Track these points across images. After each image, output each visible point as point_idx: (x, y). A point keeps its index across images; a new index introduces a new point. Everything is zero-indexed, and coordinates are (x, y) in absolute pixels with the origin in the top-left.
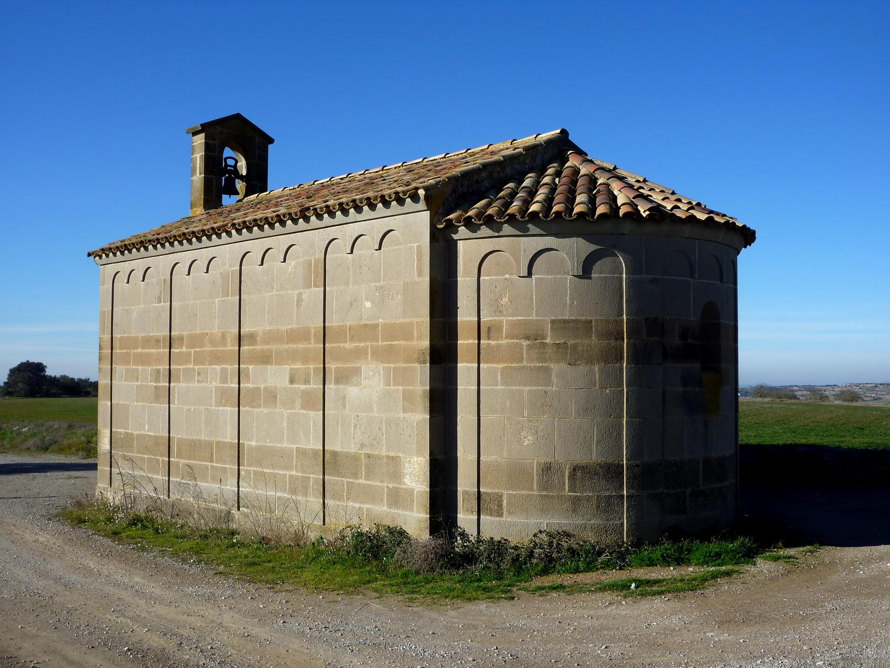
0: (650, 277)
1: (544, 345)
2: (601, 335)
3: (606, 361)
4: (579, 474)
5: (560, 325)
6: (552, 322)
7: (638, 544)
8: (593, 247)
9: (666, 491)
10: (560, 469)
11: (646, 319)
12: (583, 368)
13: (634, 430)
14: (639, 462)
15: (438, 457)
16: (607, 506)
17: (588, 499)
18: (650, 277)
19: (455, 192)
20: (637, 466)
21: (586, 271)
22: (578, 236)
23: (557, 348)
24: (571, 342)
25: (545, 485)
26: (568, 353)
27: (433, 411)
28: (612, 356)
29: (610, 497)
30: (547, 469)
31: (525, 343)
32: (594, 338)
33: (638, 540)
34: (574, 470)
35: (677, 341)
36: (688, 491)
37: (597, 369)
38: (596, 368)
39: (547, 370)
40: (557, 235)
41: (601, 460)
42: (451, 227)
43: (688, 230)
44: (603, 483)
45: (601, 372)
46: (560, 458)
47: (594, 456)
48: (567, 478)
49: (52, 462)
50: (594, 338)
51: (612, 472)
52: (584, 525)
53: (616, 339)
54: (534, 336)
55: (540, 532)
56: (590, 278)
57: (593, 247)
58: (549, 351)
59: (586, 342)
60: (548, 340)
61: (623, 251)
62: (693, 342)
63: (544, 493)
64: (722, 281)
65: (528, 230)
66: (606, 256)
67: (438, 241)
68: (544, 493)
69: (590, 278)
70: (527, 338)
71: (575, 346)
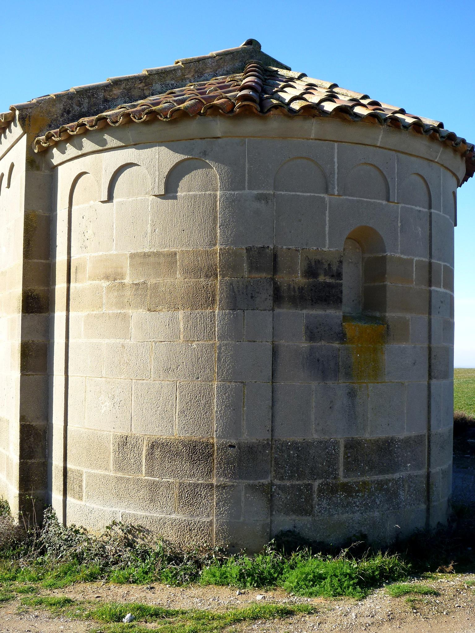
0: (255, 192)
1: (123, 285)
2: (186, 272)
3: (193, 307)
4: (157, 453)
5: (141, 259)
6: (133, 256)
7: (231, 550)
8: (179, 157)
9: (277, 482)
10: (136, 446)
11: (248, 250)
12: (164, 315)
13: (228, 398)
14: (234, 442)
15: (34, 424)
16: (189, 497)
17: (169, 486)
18: (255, 192)
19: (68, 112)
20: (231, 446)
21: (170, 187)
22: (160, 143)
23: (137, 290)
24: (152, 281)
25: (120, 466)
26: (149, 297)
27: (25, 367)
28: (201, 299)
29: (196, 486)
30: (124, 443)
31: (105, 284)
32: (178, 276)
33: (232, 546)
34: (153, 446)
35: (299, 279)
36: (316, 484)
37: (181, 317)
38: (181, 314)
39: (125, 318)
40: (138, 145)
41: (185, 436)
42: (46, 152)
43: (313, 127)
44: (187, 466)
45: (187, 319)
46: (137, 431)
47: (176, 431)
48: (144, 457)
49: (54, 421)
50: (178, 276)
51: (198, 452)
52: (164, 520)
53: (207, 276)
54: (114, 277)
55: (114, 523)
56: (175, 198)
57: (179, 157)
58: (128, 293)
59: (169, 280)
60: (127, 280)
61: (216, 160)
62: (328, 280)
63: (119, 475)
64: (388, 200)
65: (105, 142)
66: (196, 169)
67: (38, 168)
68: (119, 475)
69: (175, 198)
70: (107, 278)
71: (156, 287)
